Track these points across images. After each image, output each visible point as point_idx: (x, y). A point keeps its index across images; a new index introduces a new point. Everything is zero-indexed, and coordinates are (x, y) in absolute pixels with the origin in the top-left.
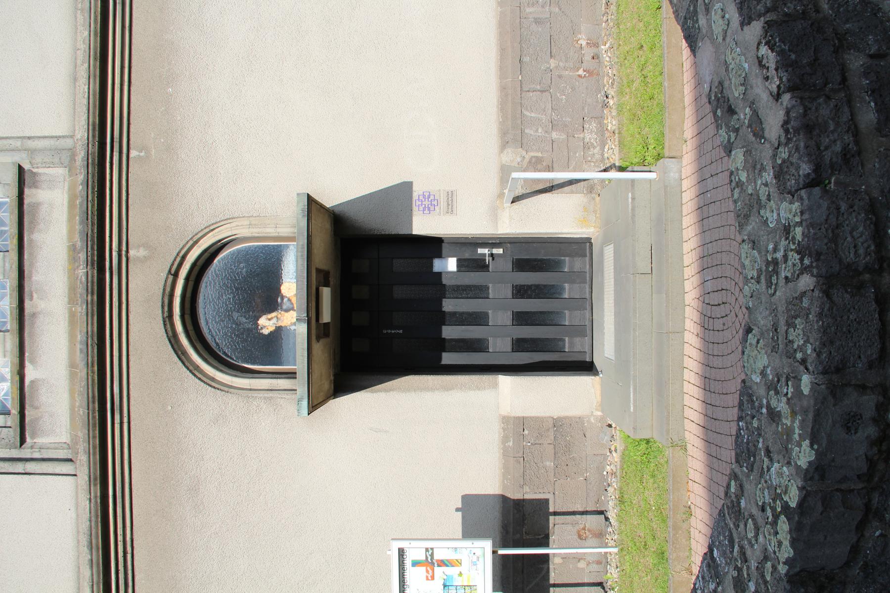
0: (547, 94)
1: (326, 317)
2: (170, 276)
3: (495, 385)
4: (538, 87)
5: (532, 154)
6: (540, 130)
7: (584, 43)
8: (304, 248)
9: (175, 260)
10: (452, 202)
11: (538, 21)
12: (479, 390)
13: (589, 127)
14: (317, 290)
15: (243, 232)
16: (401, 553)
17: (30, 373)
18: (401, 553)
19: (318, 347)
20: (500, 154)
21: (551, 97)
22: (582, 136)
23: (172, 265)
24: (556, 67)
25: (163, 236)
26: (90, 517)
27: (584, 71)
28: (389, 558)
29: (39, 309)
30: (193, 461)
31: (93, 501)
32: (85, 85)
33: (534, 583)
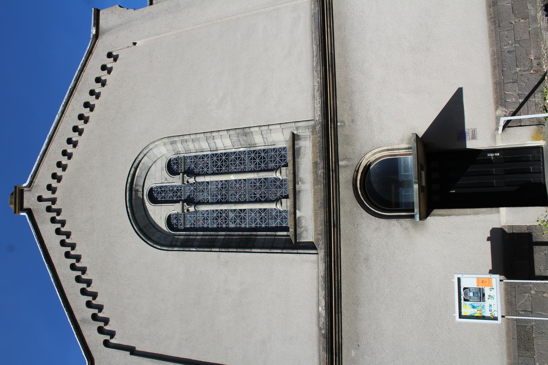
1: (424, 184)
2: (355, 172)
3: (499, 212)
7: (532, 58)
8: (416, 155)
9: (357, 165)
10: (475, 134)
11: (509, 52)
12: (491, 214)
13: (537, 96)
14: (420, 172)
15: (372, 159)
16: (459, 280)
17: (298, 214)
18: (459, 280)
19: (421, 194)
20: (495, 112)
21: (518, 85)
22: (534, 100)
23: (356, 167)
25: (352, 156)
26: (325, 269)
27: (533, 71)
28: (453, 283)
29: (301, 189)
30: (366, 247)
31: (326, 263)
32: (319, 99)
33: (521, 303)
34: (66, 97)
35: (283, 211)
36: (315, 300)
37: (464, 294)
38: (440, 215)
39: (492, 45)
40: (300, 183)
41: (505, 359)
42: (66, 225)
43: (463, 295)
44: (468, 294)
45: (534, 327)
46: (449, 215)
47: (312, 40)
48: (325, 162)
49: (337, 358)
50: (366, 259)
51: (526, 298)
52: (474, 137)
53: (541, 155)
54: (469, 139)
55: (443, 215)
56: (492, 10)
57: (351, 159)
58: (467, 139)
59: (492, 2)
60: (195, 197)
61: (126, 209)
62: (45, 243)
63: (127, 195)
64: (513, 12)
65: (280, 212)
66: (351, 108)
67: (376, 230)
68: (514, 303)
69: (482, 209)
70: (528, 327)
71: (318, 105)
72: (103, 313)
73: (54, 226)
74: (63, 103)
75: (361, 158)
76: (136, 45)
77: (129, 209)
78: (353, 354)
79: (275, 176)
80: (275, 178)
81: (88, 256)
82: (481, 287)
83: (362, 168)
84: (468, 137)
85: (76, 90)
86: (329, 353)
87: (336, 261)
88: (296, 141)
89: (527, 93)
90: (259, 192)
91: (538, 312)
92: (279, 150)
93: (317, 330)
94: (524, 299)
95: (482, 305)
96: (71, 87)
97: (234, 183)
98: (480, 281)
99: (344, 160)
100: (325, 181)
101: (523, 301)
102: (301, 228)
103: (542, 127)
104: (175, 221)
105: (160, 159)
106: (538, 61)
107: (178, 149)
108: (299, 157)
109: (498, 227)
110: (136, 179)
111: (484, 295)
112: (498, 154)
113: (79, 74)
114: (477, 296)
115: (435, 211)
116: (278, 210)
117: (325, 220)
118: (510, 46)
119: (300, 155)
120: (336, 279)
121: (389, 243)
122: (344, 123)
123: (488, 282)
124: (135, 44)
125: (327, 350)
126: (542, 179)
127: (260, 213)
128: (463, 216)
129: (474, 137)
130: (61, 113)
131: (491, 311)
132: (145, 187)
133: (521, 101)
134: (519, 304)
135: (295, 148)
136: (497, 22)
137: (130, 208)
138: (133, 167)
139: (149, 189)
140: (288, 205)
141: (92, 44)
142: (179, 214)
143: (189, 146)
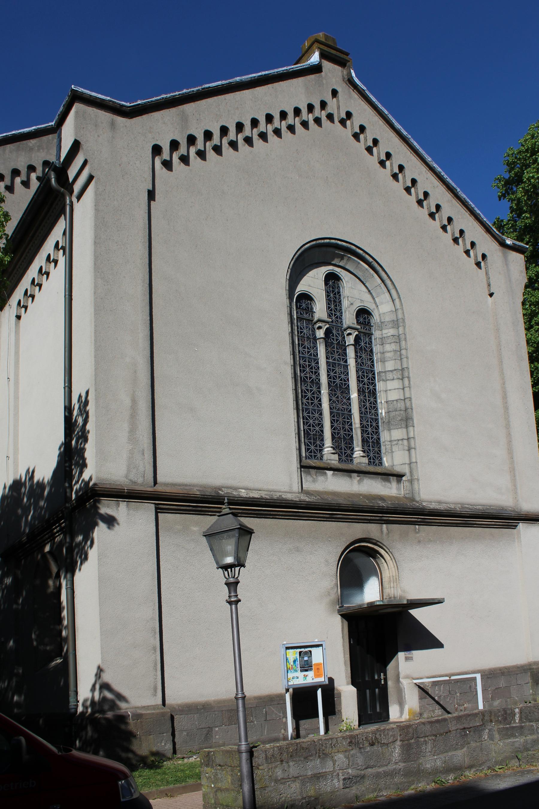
0: (449, 693)
4: (450, 690)
5: (430, 690)
6: (437, 692)
7: (465, 705)
11: (470, 687)
12: (346, 677)
17: (330, 473)
23: (381, 543)
24: (457, 696)
26: (293, 501)
33: (273, 710)
34: (448, 180)
35: (321, 454)
36: (251, 485)
37: (306, 652)
38: (343, 628)
39: (179, 706)
40: (359, 478)
41: (213, 699)
42: (303, 129)
43: (305, 651)
44: (306, 655)
45: (252, 724)
46: (343, 637)
47: (484, 506)
48: (393, 510)
49: (191, 508)
50: (298, 550)
51: (278, 714)
52: (407, 659)
53: (382, 720)
54: (405, 655)
55: (343, 631)
56: (499, 671)
57: (388, 538)
58: (405, 652)
59: (504, 672)
60: (331, 340)
61: (329, 237)
62: (280, 82)
63: (344, 244)
64: (497, 688)
65: (321, 451)
66: (430, 541)
67: (327, 561)
68: (272, 704)
69: (350, 668)
70: (251, 718)
71: (433, 506)
72: (195, 158)
73: (304, 108)
74: (443, 174)
75: (389, 548)
76: (489, 296)
77: (328, 241)
78: (193, 528)
79: (326, 446)
80: (353, 448)
81: (268, 155)
82: (313, 668)
83: (378, 549)
84: (407, 654)
85: (453, 197)
86: (201, 498)
87: (298, 514)
88: (396, 478)
89: (441, 703)
90: (340, 426)
91: (266, 726)
92: (379, 456)
93: (217, 485)
94: (277, 713)
95: (297, 669)
96: (458, 191)
97: (347, 396)
98: (318, 667)
99: (387, 530)
100: (377, 507)
101: (275, 711)
102: (316, 475)
103: (418, 717)
104: (304, 305)
105: (370, 299)
106: (463, 710)
107: (385, 329)
108: (382, 479)
109: (335, 685)
110: (357, 261)
111: (306, 671)
112: (383, 683)
113: (470, 207)
114: (305, 664)
115: (346, 623)
116: (322, 448)
117: (341, 505)
118: (474, 687)
119: (384, 482)
120: (279, 513)
121: (315, 575)
122: (417, 533)
123: (318, 674)
124: (491, 295)
125: (205, 496)
126: (364, 722)
127: (319, 424)
128: (343, 651)
129: (407, 659)
130: (432, 166)
131: (293, 679)
132: (342, 270)
133: (436, 698)
134: (272, 708)
135: (390, 477)
136: (491, 676)
137: (329, 243)
138: (373, 261)
139: (340, 276)
140: (333, 462)
141: (497, 236)
142: (313, 313)
143: (389, 345)
